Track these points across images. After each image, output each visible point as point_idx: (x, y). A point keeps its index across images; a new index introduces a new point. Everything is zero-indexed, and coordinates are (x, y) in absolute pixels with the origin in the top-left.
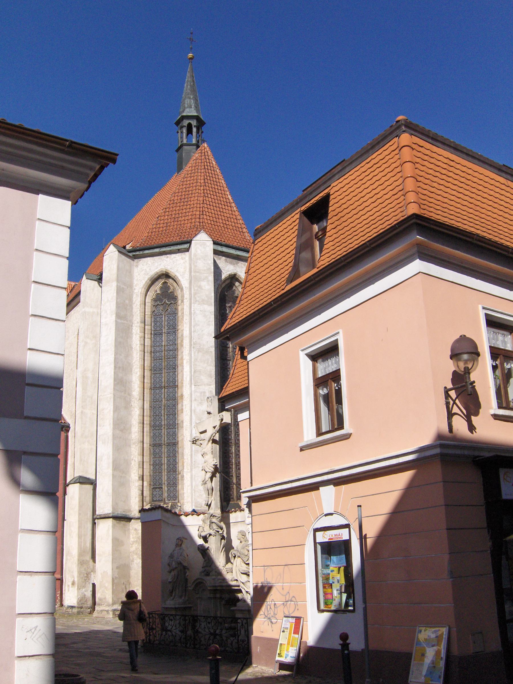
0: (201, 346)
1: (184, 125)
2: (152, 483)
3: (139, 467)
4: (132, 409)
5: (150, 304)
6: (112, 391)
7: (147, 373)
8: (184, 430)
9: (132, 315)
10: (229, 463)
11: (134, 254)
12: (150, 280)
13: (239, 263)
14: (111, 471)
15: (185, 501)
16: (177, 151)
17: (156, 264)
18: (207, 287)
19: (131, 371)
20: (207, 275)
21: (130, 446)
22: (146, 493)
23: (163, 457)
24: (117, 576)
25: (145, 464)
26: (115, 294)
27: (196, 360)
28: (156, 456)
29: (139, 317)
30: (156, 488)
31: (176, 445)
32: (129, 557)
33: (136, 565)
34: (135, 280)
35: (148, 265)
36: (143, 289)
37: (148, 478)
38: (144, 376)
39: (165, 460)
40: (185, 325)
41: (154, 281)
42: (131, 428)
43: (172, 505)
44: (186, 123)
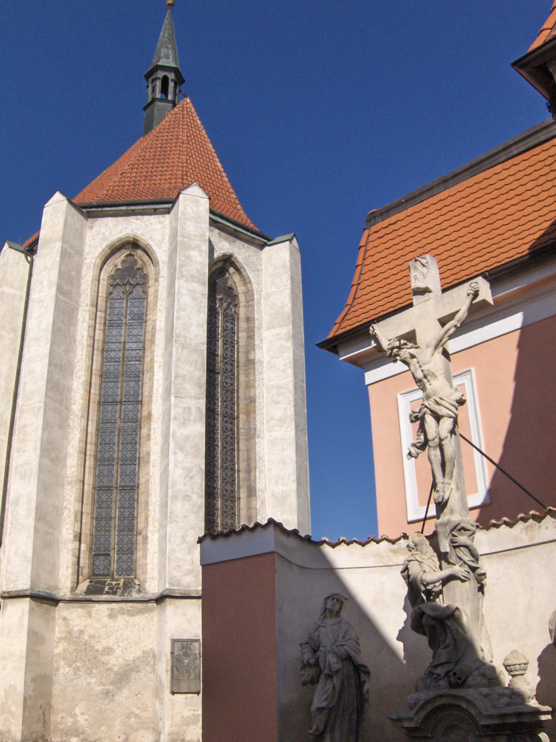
0: (188, 341)
1: (158, 76)
2: (93, 547)
3: (76, 520)
4: (70, 430)
5: (106, 283)
6: (43, 398)
7: (96, 380)
8: (151, 467)
9: (79, 294)
10: (213, 523)
11: (88, 210)
12: (110, 248)
13: (236, 241)
14: (33, 522)
15: (148, 576)
16: (145, 108)
17: (120, 227)
18: (199, 259)
19: (72, 374)
20: (200, 243)
21: (62, 486)
22: (84, 561)
23: (114, 508)
24: (32, 694)
25: (84, 515)
26: (58, 259)
27: (178, 359)
28: (103, 506)
29: (89, 298)
30: (100, 555)
31: (134, 490)
32: (52, 663)
33: (62, 676)
34: (86, 246)
35: (108, 227)
36: (98, 260)
37: (89, 538)
38: (91, 384)
39: (116, 513)
40: (159, 314)
41: (114, 250)
42: (66, 459)
43: (124, 582)
44: (161, 74)
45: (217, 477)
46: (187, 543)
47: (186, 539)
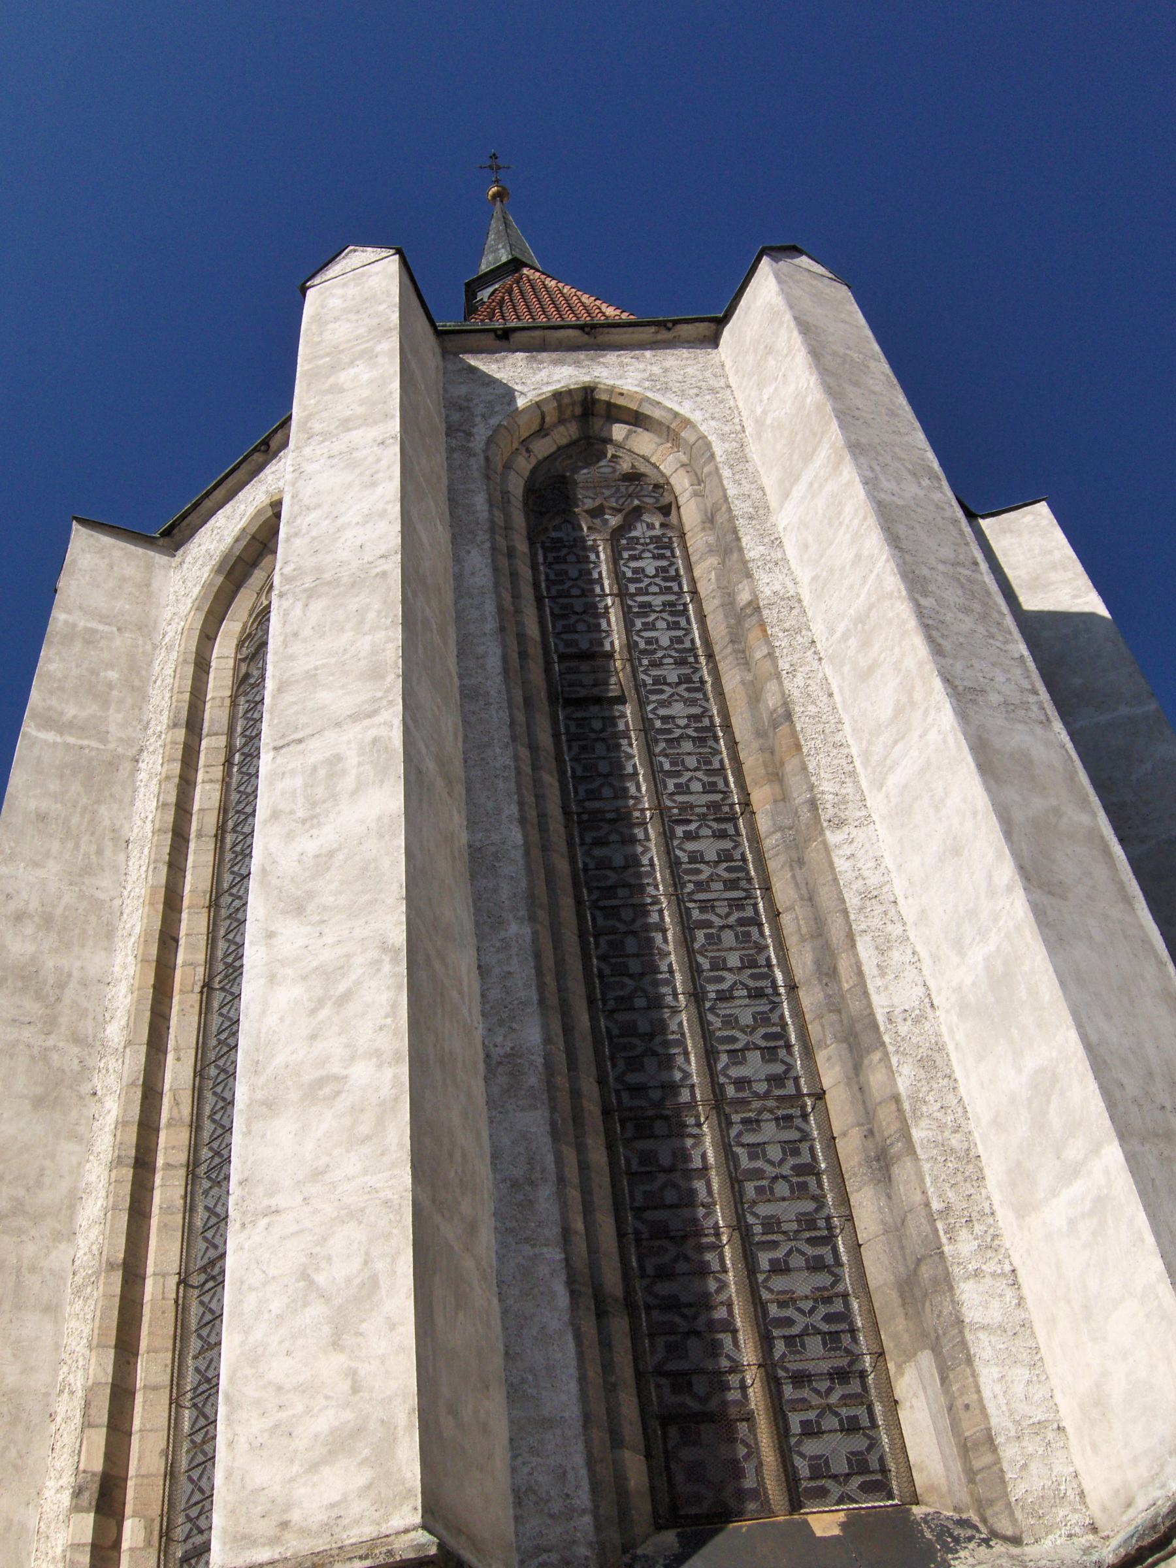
45: (681, 1043)
46: (324, 1296)
47: (320, 1279)
